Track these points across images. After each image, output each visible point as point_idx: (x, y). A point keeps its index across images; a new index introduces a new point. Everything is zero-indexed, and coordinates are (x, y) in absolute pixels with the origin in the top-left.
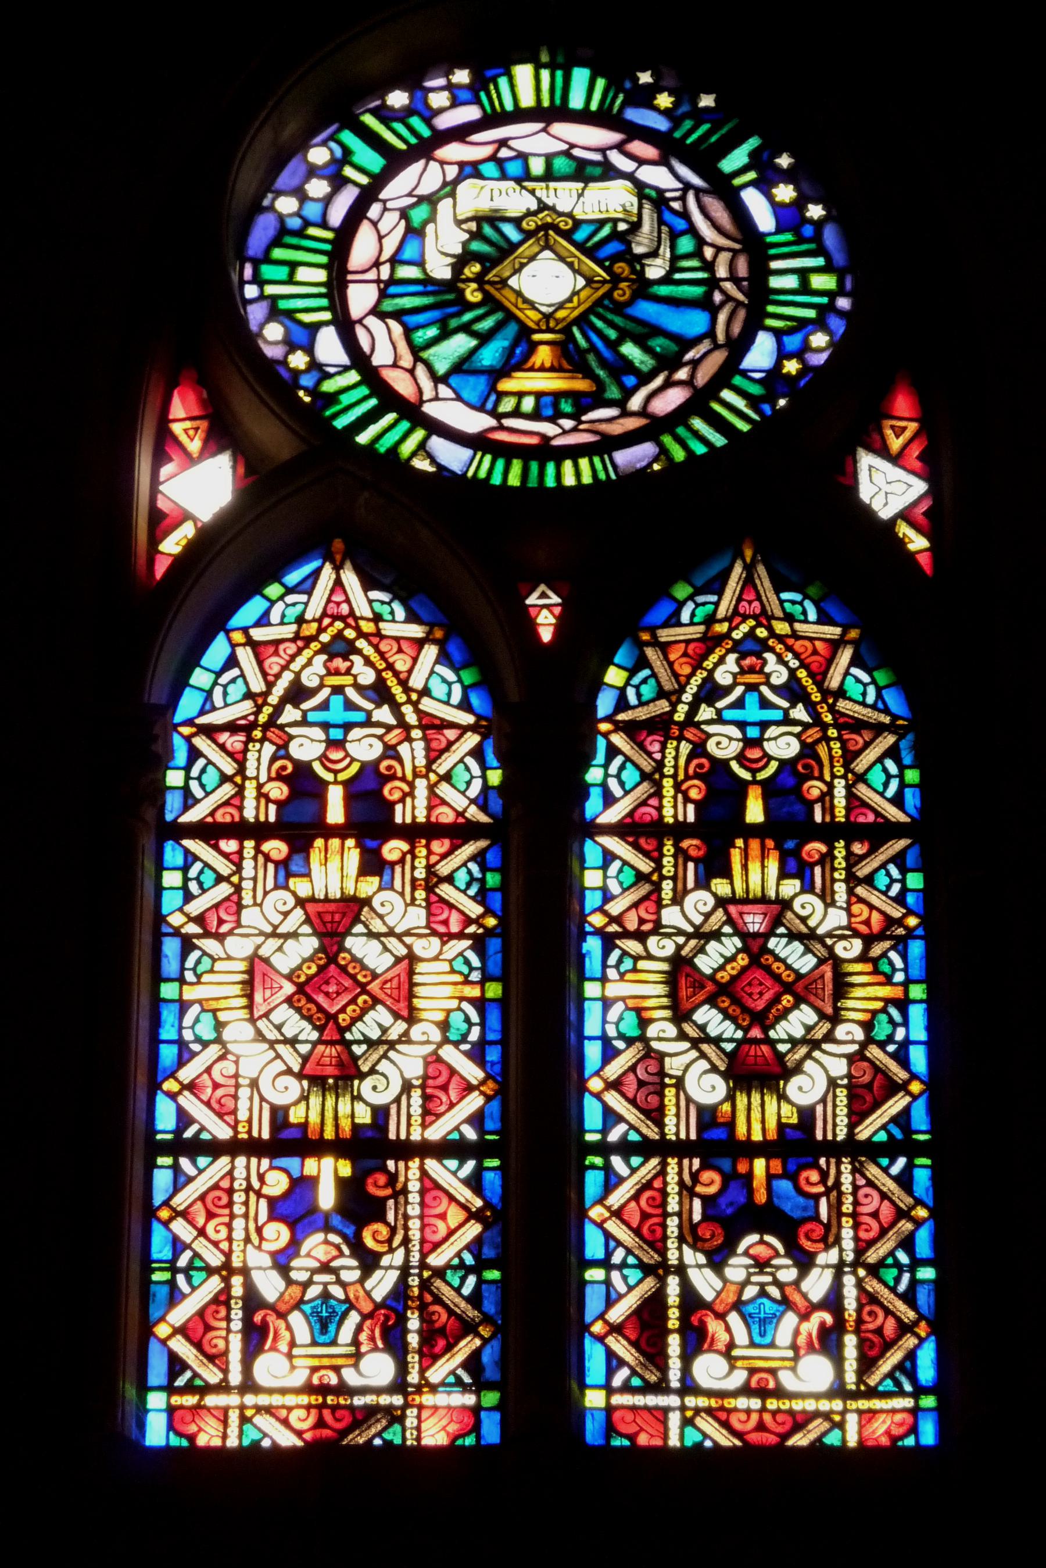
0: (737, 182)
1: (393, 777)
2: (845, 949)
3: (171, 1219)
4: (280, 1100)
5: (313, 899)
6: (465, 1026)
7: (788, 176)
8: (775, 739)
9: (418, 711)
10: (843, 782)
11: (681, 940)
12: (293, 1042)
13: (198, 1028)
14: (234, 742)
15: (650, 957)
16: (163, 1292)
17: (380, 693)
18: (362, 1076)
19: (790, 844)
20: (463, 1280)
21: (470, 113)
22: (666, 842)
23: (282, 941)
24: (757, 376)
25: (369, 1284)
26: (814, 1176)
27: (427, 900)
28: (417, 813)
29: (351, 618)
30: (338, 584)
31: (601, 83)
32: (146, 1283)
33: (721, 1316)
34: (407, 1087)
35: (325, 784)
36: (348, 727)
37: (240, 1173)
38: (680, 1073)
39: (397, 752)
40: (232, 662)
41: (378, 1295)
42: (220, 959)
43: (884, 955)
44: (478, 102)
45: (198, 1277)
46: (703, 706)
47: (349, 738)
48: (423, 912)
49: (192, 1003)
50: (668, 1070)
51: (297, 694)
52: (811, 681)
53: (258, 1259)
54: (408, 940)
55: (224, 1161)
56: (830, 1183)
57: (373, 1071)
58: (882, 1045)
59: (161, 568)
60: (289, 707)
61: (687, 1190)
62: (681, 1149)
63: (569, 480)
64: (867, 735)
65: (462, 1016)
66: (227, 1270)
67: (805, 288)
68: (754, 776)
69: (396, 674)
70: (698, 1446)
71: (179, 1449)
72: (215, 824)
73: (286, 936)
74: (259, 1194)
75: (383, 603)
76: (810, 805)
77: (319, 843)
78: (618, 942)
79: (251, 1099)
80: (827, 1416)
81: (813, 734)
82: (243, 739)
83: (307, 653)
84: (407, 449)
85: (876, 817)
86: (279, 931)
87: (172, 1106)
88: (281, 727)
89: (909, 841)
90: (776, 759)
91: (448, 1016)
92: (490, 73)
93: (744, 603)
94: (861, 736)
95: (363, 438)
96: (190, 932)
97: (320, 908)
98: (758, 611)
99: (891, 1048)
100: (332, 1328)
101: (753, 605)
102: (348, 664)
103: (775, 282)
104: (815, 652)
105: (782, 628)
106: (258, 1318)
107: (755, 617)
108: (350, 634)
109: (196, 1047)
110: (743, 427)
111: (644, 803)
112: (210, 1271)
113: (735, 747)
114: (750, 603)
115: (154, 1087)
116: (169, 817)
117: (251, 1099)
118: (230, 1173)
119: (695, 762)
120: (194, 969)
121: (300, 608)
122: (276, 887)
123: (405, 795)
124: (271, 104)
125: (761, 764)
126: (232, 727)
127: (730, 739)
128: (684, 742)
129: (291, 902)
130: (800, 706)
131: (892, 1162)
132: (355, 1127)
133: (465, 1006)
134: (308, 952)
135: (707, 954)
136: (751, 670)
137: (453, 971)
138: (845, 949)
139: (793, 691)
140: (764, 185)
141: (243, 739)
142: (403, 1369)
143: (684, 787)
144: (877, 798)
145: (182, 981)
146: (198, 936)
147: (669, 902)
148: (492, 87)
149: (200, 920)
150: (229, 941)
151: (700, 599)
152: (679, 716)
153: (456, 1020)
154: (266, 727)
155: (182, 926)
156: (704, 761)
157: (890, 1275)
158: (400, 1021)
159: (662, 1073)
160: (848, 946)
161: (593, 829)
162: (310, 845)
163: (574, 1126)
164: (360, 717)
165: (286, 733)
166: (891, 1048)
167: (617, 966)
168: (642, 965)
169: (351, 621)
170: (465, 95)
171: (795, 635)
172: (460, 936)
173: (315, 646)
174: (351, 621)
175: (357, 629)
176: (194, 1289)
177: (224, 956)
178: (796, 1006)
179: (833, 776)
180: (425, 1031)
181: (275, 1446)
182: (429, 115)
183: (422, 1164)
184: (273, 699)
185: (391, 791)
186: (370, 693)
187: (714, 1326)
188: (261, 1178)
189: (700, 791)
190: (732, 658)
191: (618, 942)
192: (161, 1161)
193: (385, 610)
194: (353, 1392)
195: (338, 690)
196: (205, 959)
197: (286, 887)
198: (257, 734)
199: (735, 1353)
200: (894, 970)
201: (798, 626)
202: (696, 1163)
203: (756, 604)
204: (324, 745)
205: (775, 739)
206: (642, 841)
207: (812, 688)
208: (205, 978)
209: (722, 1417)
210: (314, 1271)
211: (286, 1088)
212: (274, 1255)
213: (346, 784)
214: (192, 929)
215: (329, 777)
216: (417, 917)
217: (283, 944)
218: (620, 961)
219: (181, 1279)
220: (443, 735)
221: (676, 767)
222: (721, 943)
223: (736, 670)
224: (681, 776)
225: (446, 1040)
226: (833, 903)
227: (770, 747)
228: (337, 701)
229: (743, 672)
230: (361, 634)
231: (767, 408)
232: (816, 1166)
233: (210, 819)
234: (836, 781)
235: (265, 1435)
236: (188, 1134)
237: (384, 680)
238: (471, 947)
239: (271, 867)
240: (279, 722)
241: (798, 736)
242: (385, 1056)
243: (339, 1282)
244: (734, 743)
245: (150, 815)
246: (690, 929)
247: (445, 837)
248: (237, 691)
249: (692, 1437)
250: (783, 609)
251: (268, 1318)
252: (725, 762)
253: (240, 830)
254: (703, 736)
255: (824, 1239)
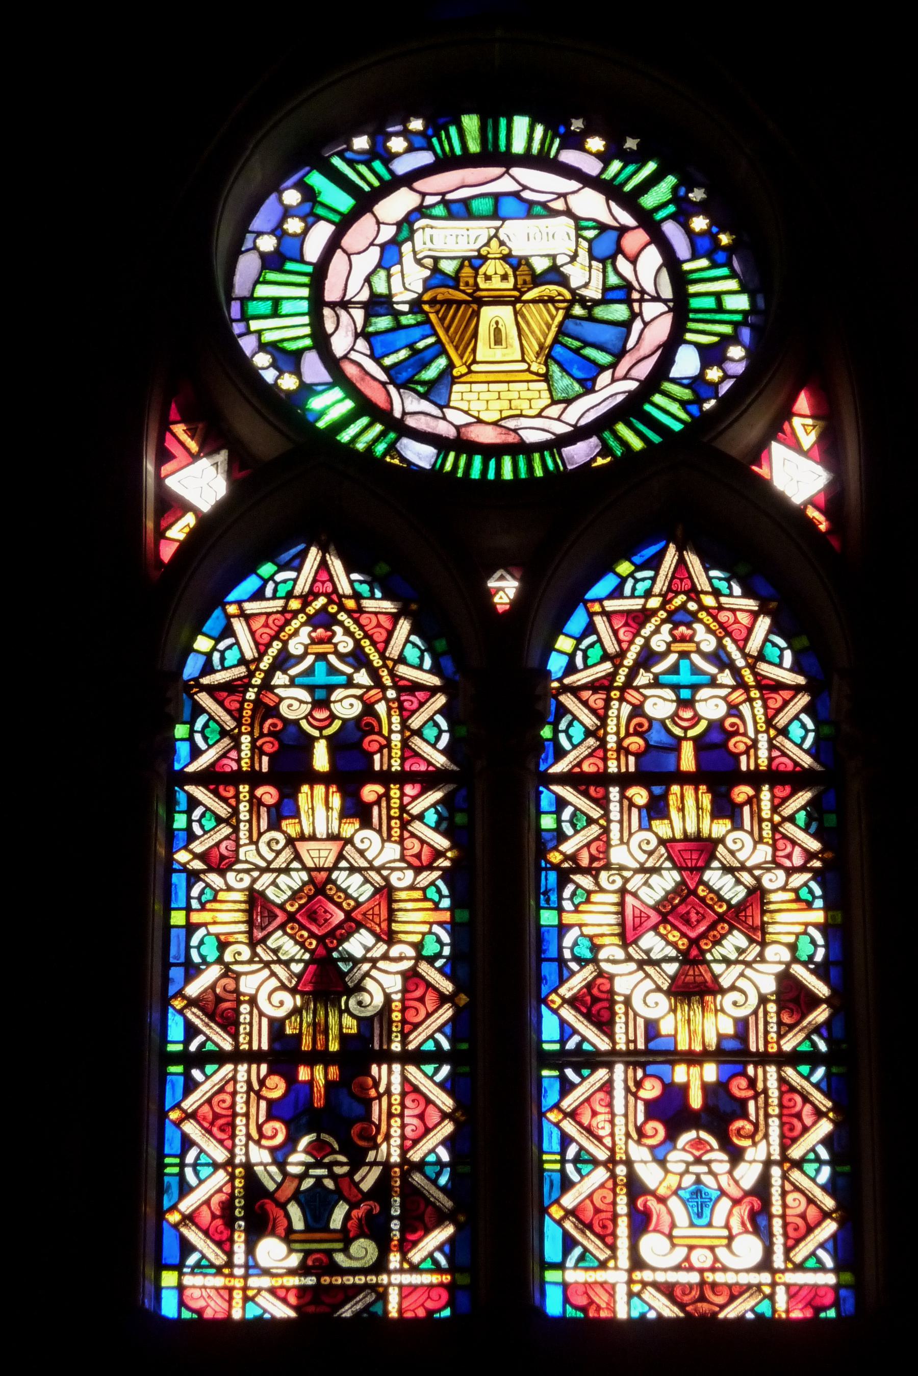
0: (659, 216)
1: (736, 733)
2: (771, 880)
3: (182, 1120)
4: (652, 1014)
5: (673, 840)
6: (812, 948)
7: (701, 208)
8: (341, 701)
9: (755, 674)
10: (765, 735)
11: (255, 874)
12: (286, 964)
13: (204, 950)
14: (597, 700)
15: (229, 889)
16: (174, 1182)
17: (358, 658)
18: (723, 991)
19: (723, 789)
20: (818, 1171)
21: (425, 158)
22: (611, 789)
23: (275, 875)
24: (685, 382)
25: (737, 1173)
26: (743, 1083)
27: (773, 838)
28: (760, 761)
29: (334, 596)
30: (682, 562)
31: (539, 130)
32: (161, 1175)
33: (662, 1200)
34: (763, 1000)
35: (314, 739)
36: (695, 688)
37: (242, 1075)
38: (253, 992)
39: (740, 711)
40: (591, 629)
41: (366, 1186)
42: (221, 890)
43: (806, 884)
44: (430, 148)
45: (204, 1172)
46: (642, 671)
47: (697, 697)
48: (769, 850)
49: (570, 926)
50: (242, 989)
51: (648, 658)
52: (373, 650)
53: (639, 1153)
54: (757, 873)
55: (229, 1067)
56: (382, 1089)
57: (733, 988)
58: (805, 964)
59: (167, 552)
60: (278, 673)
61: (631, 1093)
62: (253, 1057)
63: (507, 474)
64: (421, 695)
65: (807, 939)
66: (611, 1162)
67: (720, 309)
68: (685, 733)
69: (374, 643)
70: (643, 1316)
71: (574, 1320)
72: (583, 774)
73: (280, 871)
74: (260, 1097)
75: (720, 579)
76: (736, 757)
77: (305, 788)
78: (202, 876)
79: (251, 1013)
80: (759, 1287)
81: (738, 696)
82: (604, 696)
83: (655, 621)
84: (380, 448)
85: (428, 767)
86: (272, 867)
87: (555, 1020)
88: (637, 689)
89: (455, 786)
90: (706, 719)
91: (423, 939)
92: (442, 121)
93: (319, 584)
94: (415, 696)
95: (345, 437)
96: (196, 867)
97: (680, 846)
98: (330, 589)
99: (439, 963)
100: (707, 1211)
101: (325, 585)
102: (329, 633)
103: (695, 303)
104: (379, 625)
105: (709, 601)
106: (640, 1203)
107: (327, 595)
108: (692, 606)
109: (574, 966)
110: (677, 427)
111: (224, 755)
112: (216, 1166)
113: (306, 708)
114: (681, 580)
115: (166, 1003)
116: (177, 767)
117: (251, 1013)
118: (234, 1079)
119: (270, 721)
120: (199, 898)
121: (648, 583)
122: (270, 828)
123: (382, 748)
124: (251, 146)
125: (326, 723)
126: (594, 686)
127: (301, 702)
128: (624, 704)
129: (654, 842)
130: (363, 671)
131: (812, 1072)
132: (721, 1037)
133: (436, 929)
134: (670, 885)
135: (664, 889)
136: (683, 639)
137: (425, 899)
138: (771, 880)
139: (358, 658)
140: (682, 217)
141: (604, 696)
142: (768, 1251)
143: (258, 744)
144: (796, 750)
145: (188, 909)
146: (204, 872)
147: (247, 841)
148: (443, 133)
149: (202, 857)
150: (230, 876)
151: (639, 575)
152: (620, 680)
153: (804, 942)
154: (623, 689)
155: (188, 863)
156: (275, 720)
157: (810, 1168)
158: (380, 944)
159: (611, 992)
160: (774, 878)
161: (550, 780)
162: (298, 791)
163: (155, 1037)
164: (342, 679)
165: (641, 694)
166: (439, 963)
167: (571, 899)
168: (221, 896)
169: (335, 597)
170: (419, 141)
171: (720, 608)
172: (803, 869)
173: (302, 618)
174: (335, 597)
175: (699, 602)
176: (201, 1182)
177: (224, 887)
178: (730, 932)
179: (391, 731)
180: (777, 954)
181: (660, 1317)
182: (388, 158)
183: (403, 1070)
184: (629, 661)
185: (737, 744)
186: (351, 660)
187: (274, 1211)
188: (262, 1083)
189: (273, 745)
190: (667, 627)
191: (202, 876)
192: (172, 1069)
193: (723, 586)
194: (725, 1269)
195: (321, 657)
196: (208, 890)
197: (650, 829)
198: (615, 694)
199: (675, 1232)
200: (814, 897)
201: (723, 600)
202: (264, 1068)
203: (329, 584)
204: (675, 705)
205: (341, 701)
206: (592, 790)
207: (736, 655)
208: (208, 906)
209: (668, 1290)
210: (308, 1166)
211: (657, 1004)
212: (273, 1150)
213: (328, 738)
214: (197, 865)
215: (316, 733)
216: (764, 853)
217: (649, 878)
218: (574, 894)
219: (570, 1168)
220: (415, 696)
221: (618, 725)
222: (661, 875)
223: (669, 639)
224: (256, 734)
225: (795, 960)
226: (761, 840)
227: (336, 708)
228: (321, 667)
229: (675, 640)
230: (342, 608)
231: (694, 409)
232: (744, 1074)
233: (577, 770)
234: (760, 736)
235: (651, 1308)
236: (571, 1045)
237: (363, 648)
238: (812, 879)
239: (635, 812)
240: (635, 684)
241: (360, 698)
242: (742, 975)
243: (711, 1172)
244: (304, 706)
245: (163, 768)
246: (263, 864)
247: (787, 784)
248: (595, 654)
249: (252, 1312)
250: (711, 585)
251: (649, 1203)
252: (296, 722)
253: (603, 779)
254: (641, 699)
255: (752, 1136)
